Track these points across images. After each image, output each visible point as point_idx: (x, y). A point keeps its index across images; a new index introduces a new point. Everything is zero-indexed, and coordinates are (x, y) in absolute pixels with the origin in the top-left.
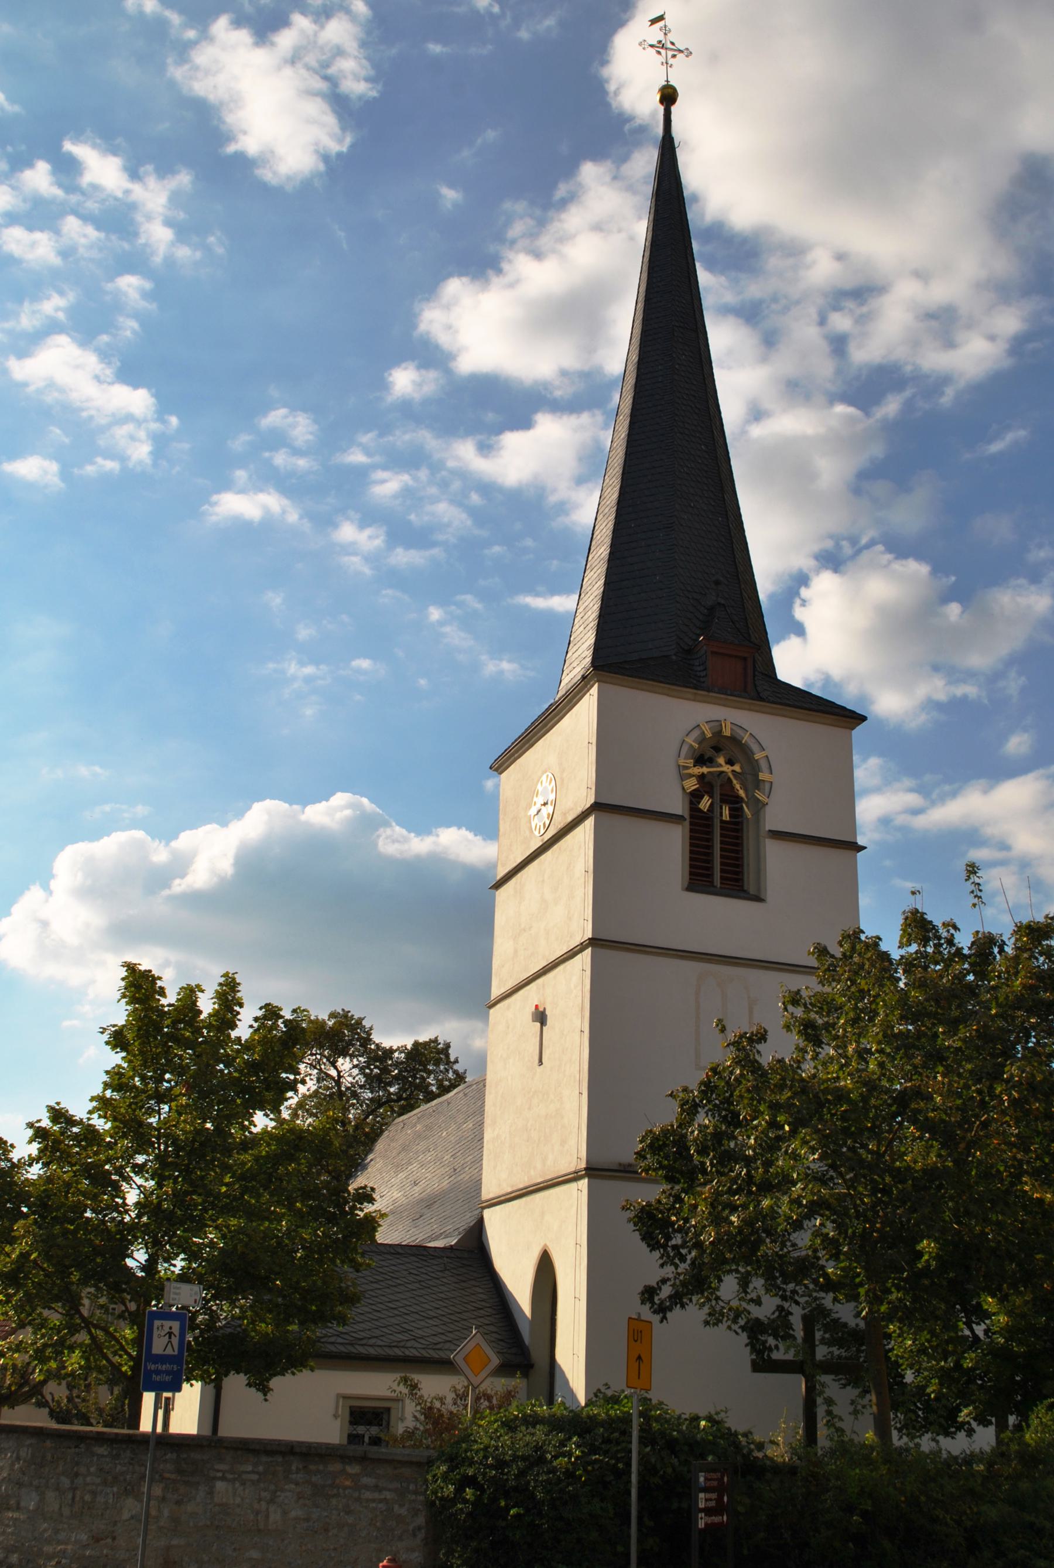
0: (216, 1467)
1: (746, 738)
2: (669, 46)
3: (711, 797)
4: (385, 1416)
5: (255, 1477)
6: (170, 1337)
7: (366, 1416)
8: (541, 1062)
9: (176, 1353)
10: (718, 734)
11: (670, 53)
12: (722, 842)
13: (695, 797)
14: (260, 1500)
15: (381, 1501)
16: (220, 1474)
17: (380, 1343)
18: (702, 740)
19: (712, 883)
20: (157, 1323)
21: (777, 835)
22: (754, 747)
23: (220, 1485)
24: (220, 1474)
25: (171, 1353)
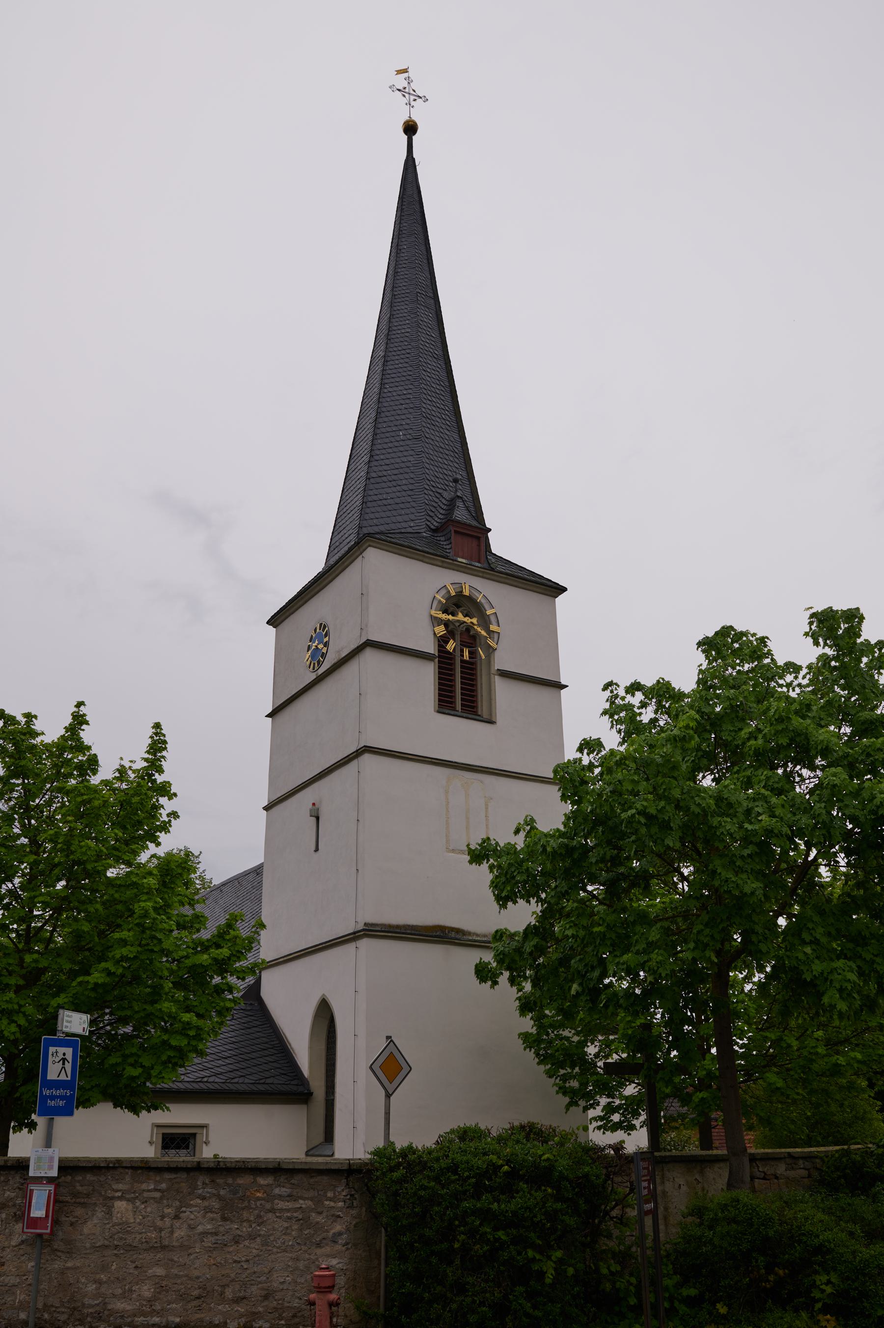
0: (115, 1187)
1: (480, 598)
2: (412, 92)
3: (454, 640)
4: (192, 1141)
5: (157, 1195)
6: (64, 1064)
7: (176, 1140)
8: (317, 850)
9: (69, 1078)
10: (460, 594)
11: (412, 98)
12: (462, 678)
13: (442, 641)
14: (163, 1217)
15: (296, 1210)
16: (119, 1194)
17: (187, 1079)
18: (449, 598)
19: (454, 709)
20: (52, 1049)
21: (504, 674)
22: (486, 606)
23: (120, 1206)
24: (119, 1194)
25: (66, 1078)
